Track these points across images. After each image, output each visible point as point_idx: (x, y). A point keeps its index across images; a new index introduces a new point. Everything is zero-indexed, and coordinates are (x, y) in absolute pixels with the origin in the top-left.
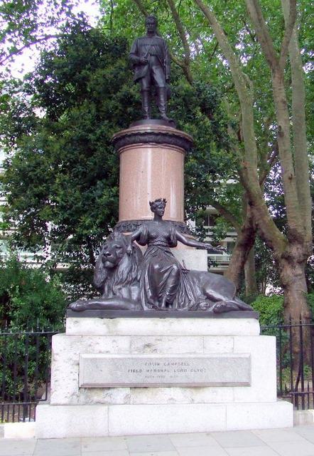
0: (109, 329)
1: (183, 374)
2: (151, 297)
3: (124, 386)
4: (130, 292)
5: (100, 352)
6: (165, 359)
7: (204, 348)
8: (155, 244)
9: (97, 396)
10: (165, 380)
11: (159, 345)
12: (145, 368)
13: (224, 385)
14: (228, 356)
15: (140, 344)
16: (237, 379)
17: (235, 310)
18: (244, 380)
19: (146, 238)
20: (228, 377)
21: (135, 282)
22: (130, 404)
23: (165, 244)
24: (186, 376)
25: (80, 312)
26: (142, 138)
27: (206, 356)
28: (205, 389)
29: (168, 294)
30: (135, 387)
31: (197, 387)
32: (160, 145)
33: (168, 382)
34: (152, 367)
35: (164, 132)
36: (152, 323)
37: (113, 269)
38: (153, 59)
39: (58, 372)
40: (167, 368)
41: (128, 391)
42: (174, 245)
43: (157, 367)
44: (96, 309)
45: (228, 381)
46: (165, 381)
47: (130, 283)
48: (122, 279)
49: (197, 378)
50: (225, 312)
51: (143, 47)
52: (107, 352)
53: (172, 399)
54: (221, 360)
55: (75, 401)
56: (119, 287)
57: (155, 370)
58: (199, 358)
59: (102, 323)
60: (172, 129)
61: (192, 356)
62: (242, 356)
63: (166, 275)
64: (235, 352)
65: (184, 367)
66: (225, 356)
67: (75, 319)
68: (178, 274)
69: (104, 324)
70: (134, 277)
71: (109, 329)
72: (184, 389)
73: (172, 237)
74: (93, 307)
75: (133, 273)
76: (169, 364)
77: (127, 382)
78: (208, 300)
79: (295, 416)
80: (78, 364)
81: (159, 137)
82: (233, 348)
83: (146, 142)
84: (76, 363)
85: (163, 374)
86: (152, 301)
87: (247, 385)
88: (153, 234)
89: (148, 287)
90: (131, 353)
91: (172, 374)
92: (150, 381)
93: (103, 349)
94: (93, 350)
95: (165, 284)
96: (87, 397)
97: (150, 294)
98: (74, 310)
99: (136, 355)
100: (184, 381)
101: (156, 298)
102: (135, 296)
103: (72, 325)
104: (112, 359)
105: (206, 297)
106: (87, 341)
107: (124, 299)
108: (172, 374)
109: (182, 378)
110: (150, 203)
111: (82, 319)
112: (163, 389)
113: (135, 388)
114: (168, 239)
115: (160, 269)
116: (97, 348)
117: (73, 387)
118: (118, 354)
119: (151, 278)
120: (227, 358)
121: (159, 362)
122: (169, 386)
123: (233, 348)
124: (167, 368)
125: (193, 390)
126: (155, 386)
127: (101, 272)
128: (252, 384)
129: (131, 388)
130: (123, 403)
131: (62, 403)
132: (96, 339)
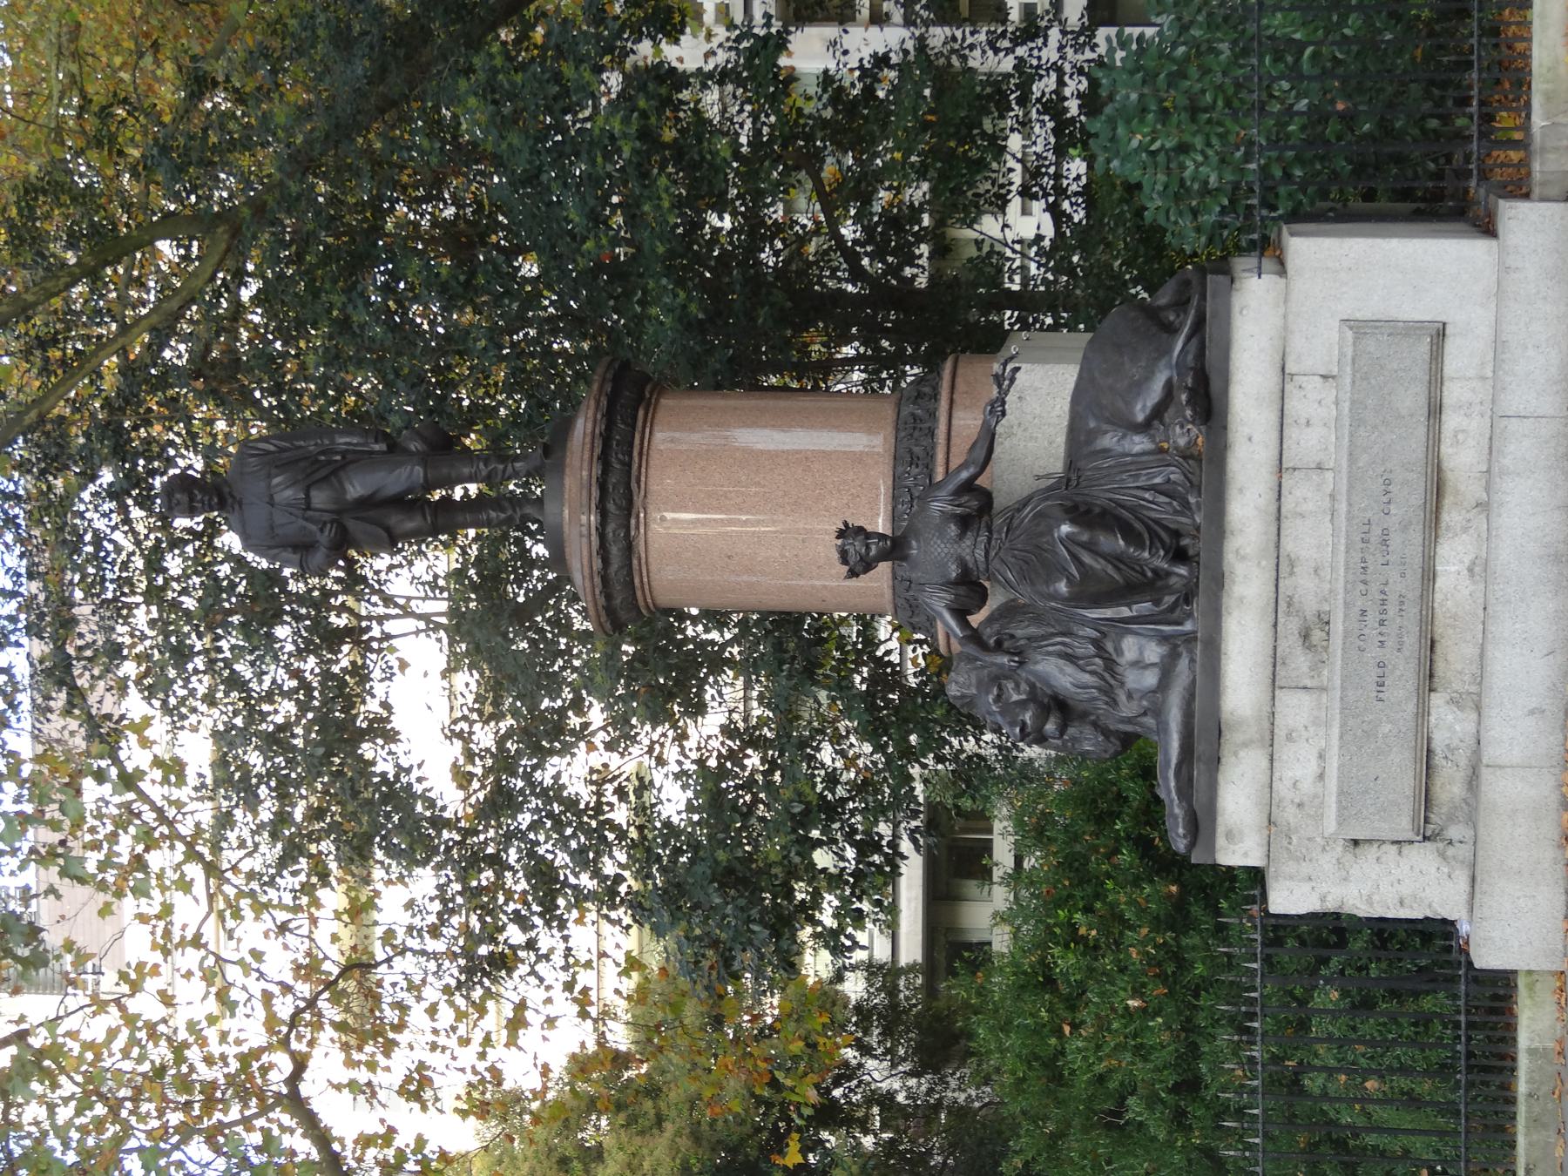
0: (1252, 741)
1: (1395, 540)
2: (1157, 602)
3: (1423, 712)
4: (1139, 664)
5: (1321, 777)
6: (1346, 591)
7: (1319, 467)
8: (982, 567)
9: (1450, 787)
10: (1410, 596)
11: (1310, 605)
12: (1373, 653)
13: (1435, 410)
14: (1346, 396)
15: (1299, 662)
16: (1421, 373)
17: (1202, 348)
18: (1424, 347)
19: (962, 590)
20: (1412, 399)
21: (1109, 646)
22: (1479, 695)
23: (983, 539)
24: (1405, 528)
25: (1201, 823)
26: (615, 565)
27: (1344, 463)
28: (1446, 465)
29: (1146, 555)
30: (1429, 679)
31: (1438, 487)
32: (638, 501)
33: (1418, 584)
34: (1372, 631)
35: (595, 493)
36: (1235, 614)
37: (1060, 707)
38: (320, 498)
39: (1376, 898)
40: (1374, 588)
41: (1437, 700)
42: (986, 497)
43: (1373, 617)
44: (1191, 779)
45: (1423, 400)
46: (1413, 594)
47: (1110, 664)
48: (1099, 689)
49: (1410, 498)
50: (1207, 395)
51: (279, 531)
52: (1321, 756)
53: (1470, 570)
54: (1357, 422)
55: (1464, 851)
56: (1122, 697)
57: (1382, 623)
58: (1351, 487)
59: (1233, 759)
60: (583, 428)
61: (1342, 507)
62: (1349, 352)
63: (1087, 558)
64: (1335, 371)
65: (1377, 531)
66: (1346, 406)
67: (1221, 841)
68: (1081, 514)
69: (1236, 754)
70: (1092, 649)
71: (1252, 741)
72: (1442, 531)
73: (959, 511)
74: (1186, 788)
75: (1080, 652)
76: (1365, 582)
77: (1411, 707)
78: (1167, 417)
79: (1543, 199)
80: (1356, 842)
81: (611, 507)
82: (1324, 377)
83: (629, 548)
84: (1351, 845)
85: (1393, 598)
86: (1169, 600)
87: (1440, 334)
88: (953, 572)
89: (1125, 612)
90: (1323, 689)
91: (1393, 574)
92: (1411, 641)
93: (1313, 767)
94: (1316, 796)
95: (1116, 560)
96: (1451, 818)
97: (1145, 607)
98: (1192, 845)
99: (1334, 673)
100: (1416, 536)
101: (1160, 583)
102: (1154, 653)
103: (1240, 848)
104: (1341, 748)
105: (1156, 423)
106: (1289, 815)
107: (1164, 684)
108: (1393, 574)
109: (1408, 544)
110: (853, 574)
111: (1220, 820)
112: (1438, 597)
113: (1431, 676)
114: (965, 523)
115: (1070, 582)
116: (1307, 786)
117: (1423, 858)
118: (1327, 725)
119: (1097, 601)
120: (1353, 402)
121: (1356, 611)
122: (1429, 575)
123: (1324, 377)
124: (1374, 588)
125: (1448, 501)
126: (1427, 619)
127: (1074, 739)
128: (1443, 318)
129: (1431, 690)
130: (1474, 716)
131: (1468, 889)
132: (1282, 789)
